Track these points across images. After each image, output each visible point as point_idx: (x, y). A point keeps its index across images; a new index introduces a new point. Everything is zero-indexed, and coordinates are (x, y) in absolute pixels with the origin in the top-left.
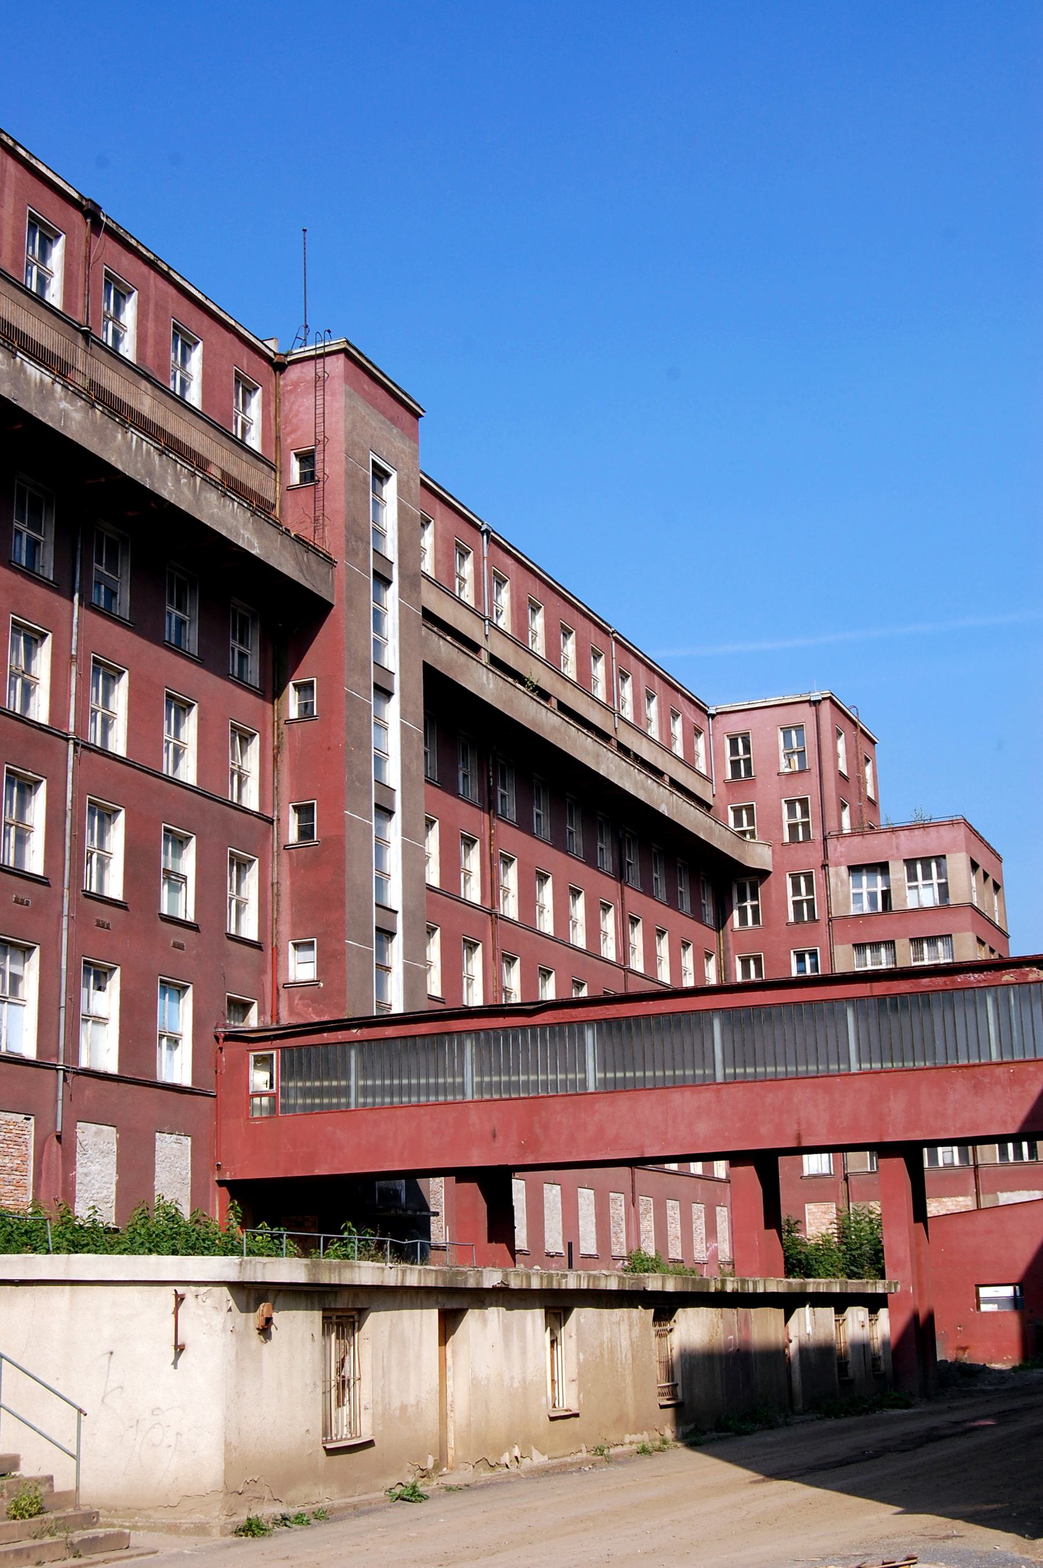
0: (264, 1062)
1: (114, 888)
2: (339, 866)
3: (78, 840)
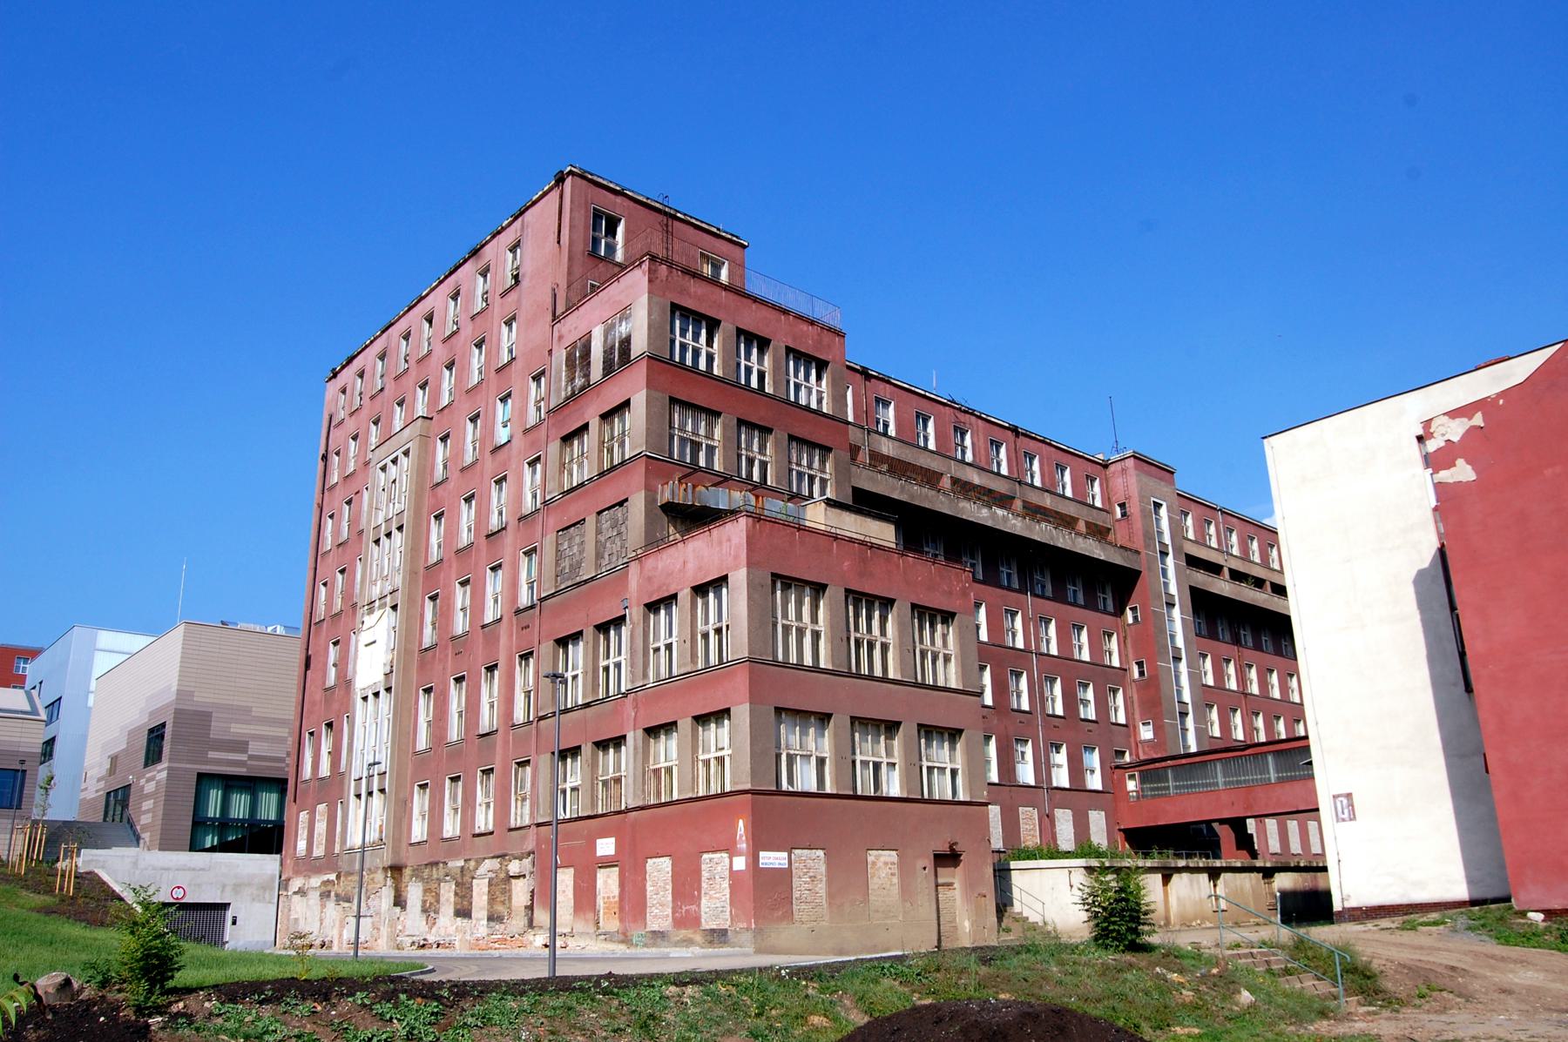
0: (1132, 777)
1: (1059, 711)
2: (1158, 688)
3: (1041, 687)
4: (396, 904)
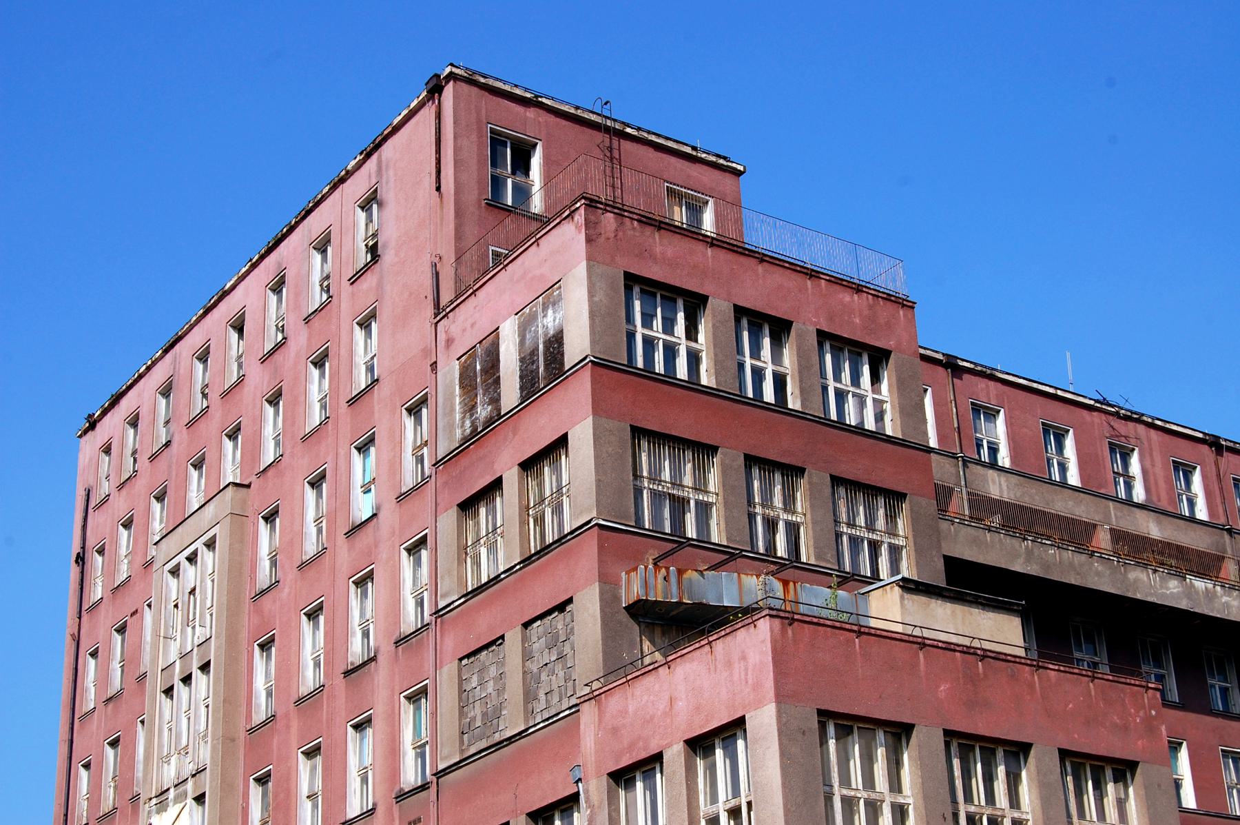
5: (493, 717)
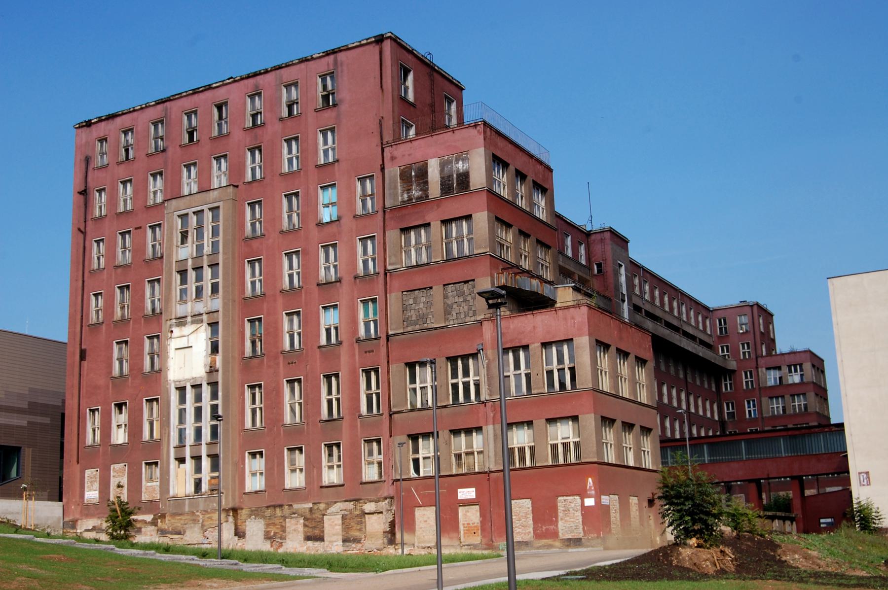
4: (236, 534)
5: (423, 318)
